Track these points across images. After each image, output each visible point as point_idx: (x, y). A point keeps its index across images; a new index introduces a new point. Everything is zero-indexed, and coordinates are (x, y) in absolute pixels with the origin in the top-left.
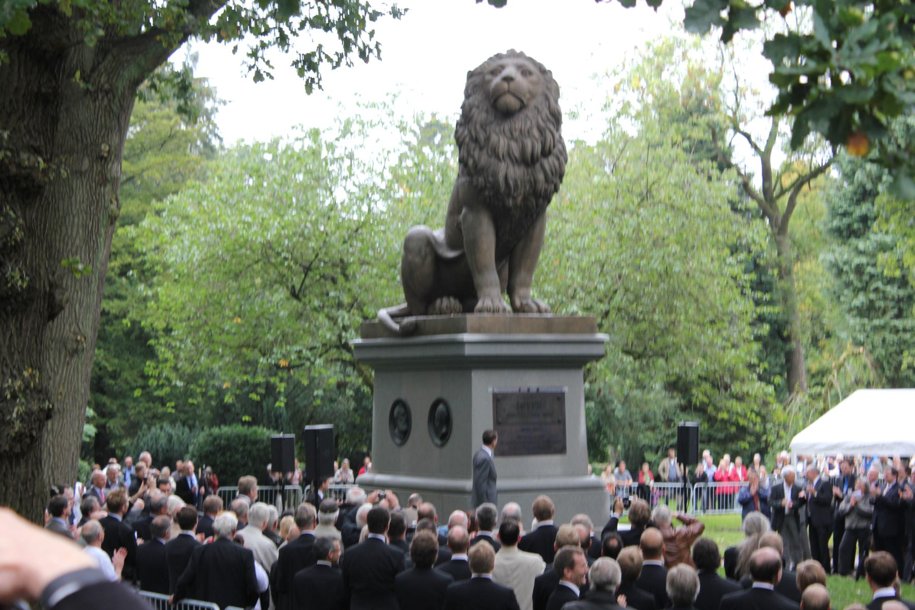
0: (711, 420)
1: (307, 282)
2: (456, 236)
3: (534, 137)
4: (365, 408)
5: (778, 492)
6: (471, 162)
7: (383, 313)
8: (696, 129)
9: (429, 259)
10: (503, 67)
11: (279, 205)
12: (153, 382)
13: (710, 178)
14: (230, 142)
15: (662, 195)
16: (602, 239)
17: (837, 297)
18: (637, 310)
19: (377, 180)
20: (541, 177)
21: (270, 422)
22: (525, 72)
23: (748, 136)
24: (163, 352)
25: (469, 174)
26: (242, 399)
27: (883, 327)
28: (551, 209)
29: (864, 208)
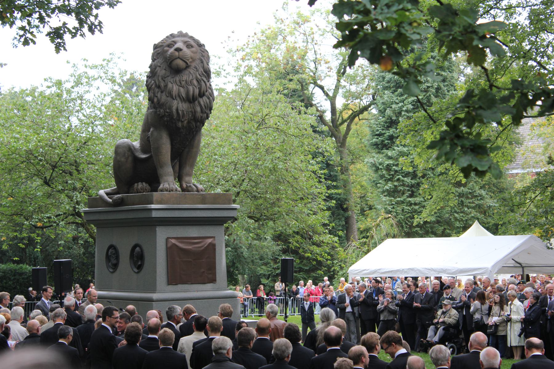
0: (302, 258)
1: (54, 174)
2: (146, 144)
3: (194, 85)
4: (90, 253)
5: (342, 299)
6: (155, 100)
7: (102, 192)
8: (291, 83)
9: (130, 159)
10: (175, 42)
11: (36, 127)
13: (300, 113)
15: (271, 122)
17: (375, 184)
18: (256, 192)
19: (98, 113)
20: (198, 109)
21: (31, 262)
22: (189, 46)
23: (322, 88)
25: (155, 107)
26: (14, 248)
27: (403, 202)
28: (205, 129)
29: (391, 131)
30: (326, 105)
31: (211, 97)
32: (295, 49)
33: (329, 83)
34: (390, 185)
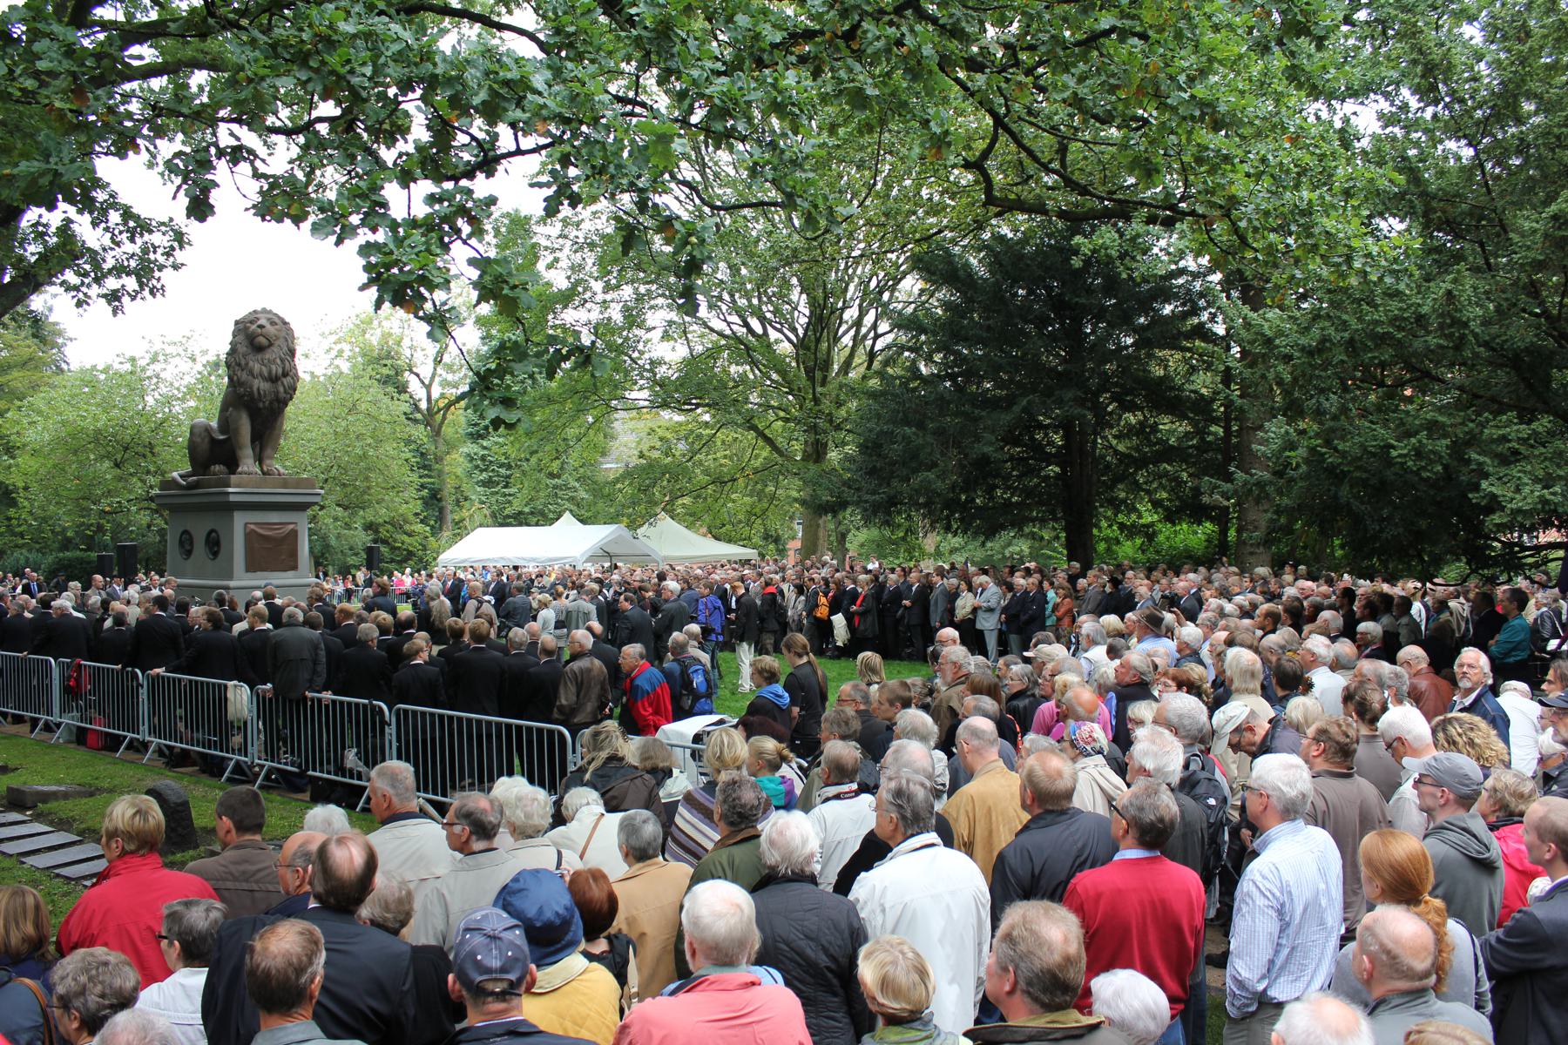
2: (225, 423)
7: (175, 474)
12: (14, 522)
14: (74, 366)
16: (324, 434)
18: (345, 479)
22: (273, 323)
28: (290, 409)
30: (421, 394)
31: (296, 377)
32: (390, 334)
33: (426, 371)
34: (485, 475)
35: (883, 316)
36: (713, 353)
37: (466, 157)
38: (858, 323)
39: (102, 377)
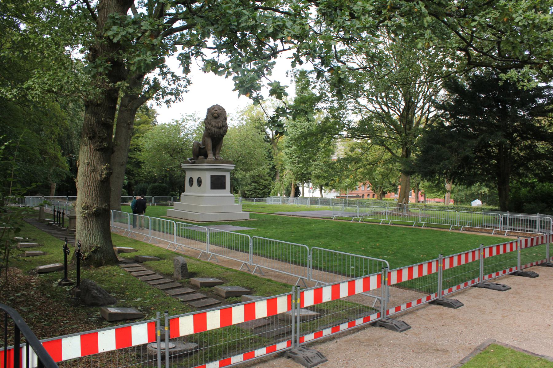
2: (204, 142)
22: (220, 109)
24: (143, 167)
28: (225, 137)
31: (227, 127)
35: (431, 105)
36: (370, 118)
37: (268, 53)
38: (422, 108)
39: (168, 127)
